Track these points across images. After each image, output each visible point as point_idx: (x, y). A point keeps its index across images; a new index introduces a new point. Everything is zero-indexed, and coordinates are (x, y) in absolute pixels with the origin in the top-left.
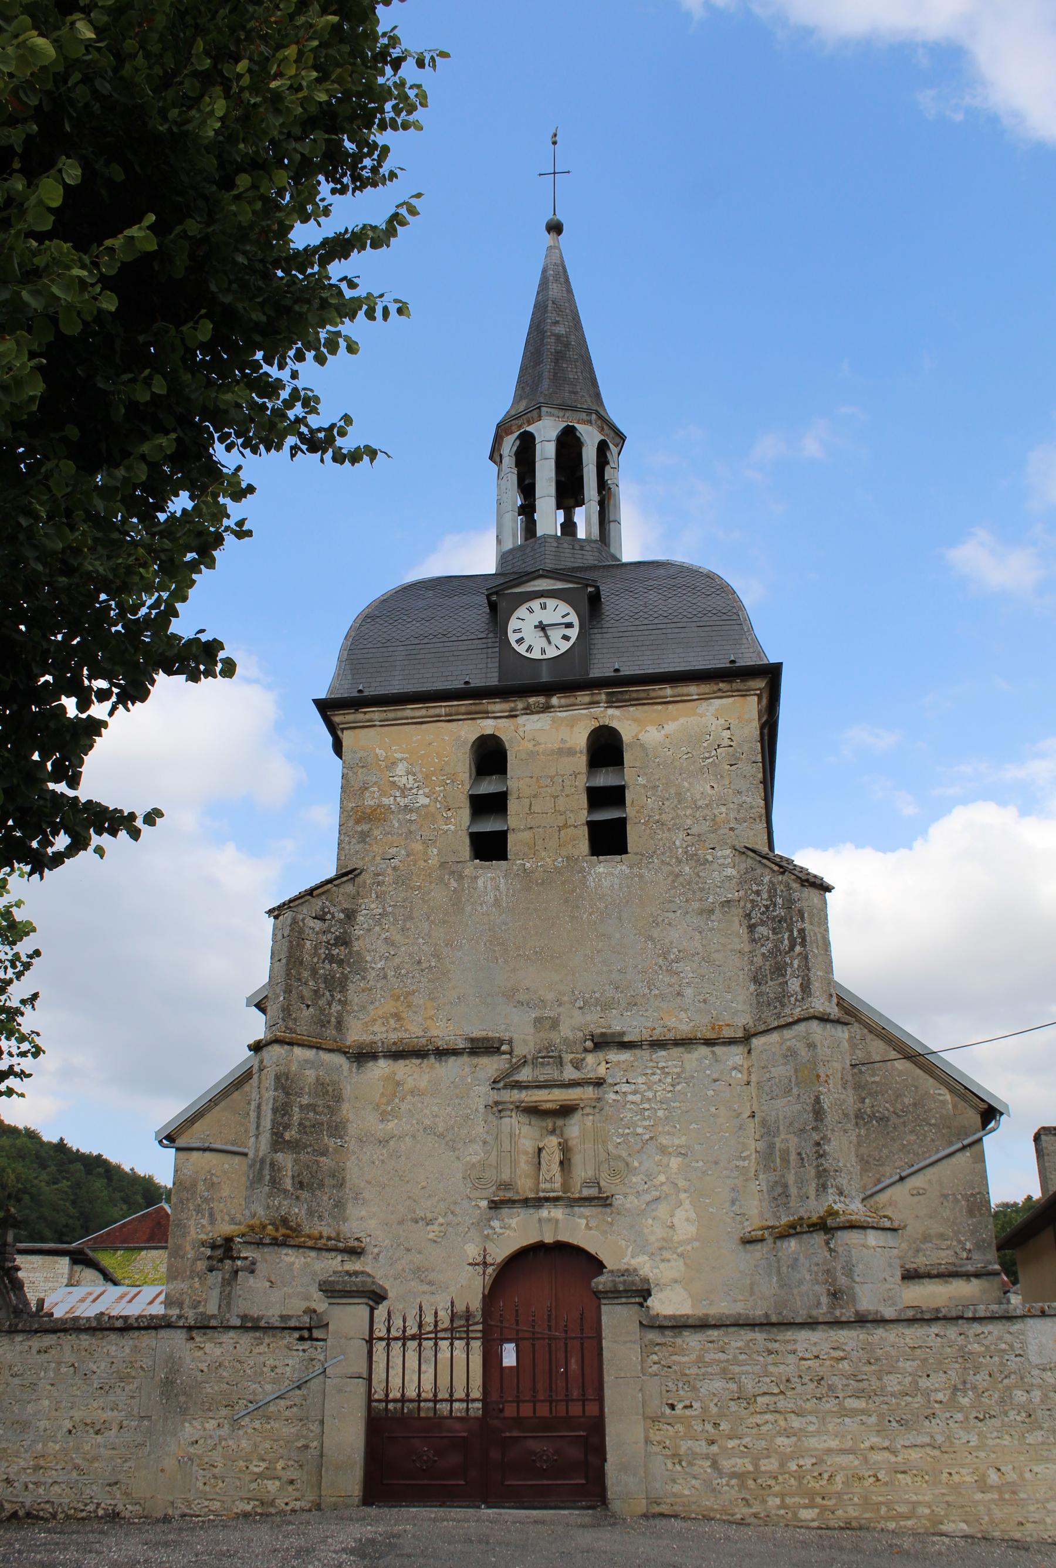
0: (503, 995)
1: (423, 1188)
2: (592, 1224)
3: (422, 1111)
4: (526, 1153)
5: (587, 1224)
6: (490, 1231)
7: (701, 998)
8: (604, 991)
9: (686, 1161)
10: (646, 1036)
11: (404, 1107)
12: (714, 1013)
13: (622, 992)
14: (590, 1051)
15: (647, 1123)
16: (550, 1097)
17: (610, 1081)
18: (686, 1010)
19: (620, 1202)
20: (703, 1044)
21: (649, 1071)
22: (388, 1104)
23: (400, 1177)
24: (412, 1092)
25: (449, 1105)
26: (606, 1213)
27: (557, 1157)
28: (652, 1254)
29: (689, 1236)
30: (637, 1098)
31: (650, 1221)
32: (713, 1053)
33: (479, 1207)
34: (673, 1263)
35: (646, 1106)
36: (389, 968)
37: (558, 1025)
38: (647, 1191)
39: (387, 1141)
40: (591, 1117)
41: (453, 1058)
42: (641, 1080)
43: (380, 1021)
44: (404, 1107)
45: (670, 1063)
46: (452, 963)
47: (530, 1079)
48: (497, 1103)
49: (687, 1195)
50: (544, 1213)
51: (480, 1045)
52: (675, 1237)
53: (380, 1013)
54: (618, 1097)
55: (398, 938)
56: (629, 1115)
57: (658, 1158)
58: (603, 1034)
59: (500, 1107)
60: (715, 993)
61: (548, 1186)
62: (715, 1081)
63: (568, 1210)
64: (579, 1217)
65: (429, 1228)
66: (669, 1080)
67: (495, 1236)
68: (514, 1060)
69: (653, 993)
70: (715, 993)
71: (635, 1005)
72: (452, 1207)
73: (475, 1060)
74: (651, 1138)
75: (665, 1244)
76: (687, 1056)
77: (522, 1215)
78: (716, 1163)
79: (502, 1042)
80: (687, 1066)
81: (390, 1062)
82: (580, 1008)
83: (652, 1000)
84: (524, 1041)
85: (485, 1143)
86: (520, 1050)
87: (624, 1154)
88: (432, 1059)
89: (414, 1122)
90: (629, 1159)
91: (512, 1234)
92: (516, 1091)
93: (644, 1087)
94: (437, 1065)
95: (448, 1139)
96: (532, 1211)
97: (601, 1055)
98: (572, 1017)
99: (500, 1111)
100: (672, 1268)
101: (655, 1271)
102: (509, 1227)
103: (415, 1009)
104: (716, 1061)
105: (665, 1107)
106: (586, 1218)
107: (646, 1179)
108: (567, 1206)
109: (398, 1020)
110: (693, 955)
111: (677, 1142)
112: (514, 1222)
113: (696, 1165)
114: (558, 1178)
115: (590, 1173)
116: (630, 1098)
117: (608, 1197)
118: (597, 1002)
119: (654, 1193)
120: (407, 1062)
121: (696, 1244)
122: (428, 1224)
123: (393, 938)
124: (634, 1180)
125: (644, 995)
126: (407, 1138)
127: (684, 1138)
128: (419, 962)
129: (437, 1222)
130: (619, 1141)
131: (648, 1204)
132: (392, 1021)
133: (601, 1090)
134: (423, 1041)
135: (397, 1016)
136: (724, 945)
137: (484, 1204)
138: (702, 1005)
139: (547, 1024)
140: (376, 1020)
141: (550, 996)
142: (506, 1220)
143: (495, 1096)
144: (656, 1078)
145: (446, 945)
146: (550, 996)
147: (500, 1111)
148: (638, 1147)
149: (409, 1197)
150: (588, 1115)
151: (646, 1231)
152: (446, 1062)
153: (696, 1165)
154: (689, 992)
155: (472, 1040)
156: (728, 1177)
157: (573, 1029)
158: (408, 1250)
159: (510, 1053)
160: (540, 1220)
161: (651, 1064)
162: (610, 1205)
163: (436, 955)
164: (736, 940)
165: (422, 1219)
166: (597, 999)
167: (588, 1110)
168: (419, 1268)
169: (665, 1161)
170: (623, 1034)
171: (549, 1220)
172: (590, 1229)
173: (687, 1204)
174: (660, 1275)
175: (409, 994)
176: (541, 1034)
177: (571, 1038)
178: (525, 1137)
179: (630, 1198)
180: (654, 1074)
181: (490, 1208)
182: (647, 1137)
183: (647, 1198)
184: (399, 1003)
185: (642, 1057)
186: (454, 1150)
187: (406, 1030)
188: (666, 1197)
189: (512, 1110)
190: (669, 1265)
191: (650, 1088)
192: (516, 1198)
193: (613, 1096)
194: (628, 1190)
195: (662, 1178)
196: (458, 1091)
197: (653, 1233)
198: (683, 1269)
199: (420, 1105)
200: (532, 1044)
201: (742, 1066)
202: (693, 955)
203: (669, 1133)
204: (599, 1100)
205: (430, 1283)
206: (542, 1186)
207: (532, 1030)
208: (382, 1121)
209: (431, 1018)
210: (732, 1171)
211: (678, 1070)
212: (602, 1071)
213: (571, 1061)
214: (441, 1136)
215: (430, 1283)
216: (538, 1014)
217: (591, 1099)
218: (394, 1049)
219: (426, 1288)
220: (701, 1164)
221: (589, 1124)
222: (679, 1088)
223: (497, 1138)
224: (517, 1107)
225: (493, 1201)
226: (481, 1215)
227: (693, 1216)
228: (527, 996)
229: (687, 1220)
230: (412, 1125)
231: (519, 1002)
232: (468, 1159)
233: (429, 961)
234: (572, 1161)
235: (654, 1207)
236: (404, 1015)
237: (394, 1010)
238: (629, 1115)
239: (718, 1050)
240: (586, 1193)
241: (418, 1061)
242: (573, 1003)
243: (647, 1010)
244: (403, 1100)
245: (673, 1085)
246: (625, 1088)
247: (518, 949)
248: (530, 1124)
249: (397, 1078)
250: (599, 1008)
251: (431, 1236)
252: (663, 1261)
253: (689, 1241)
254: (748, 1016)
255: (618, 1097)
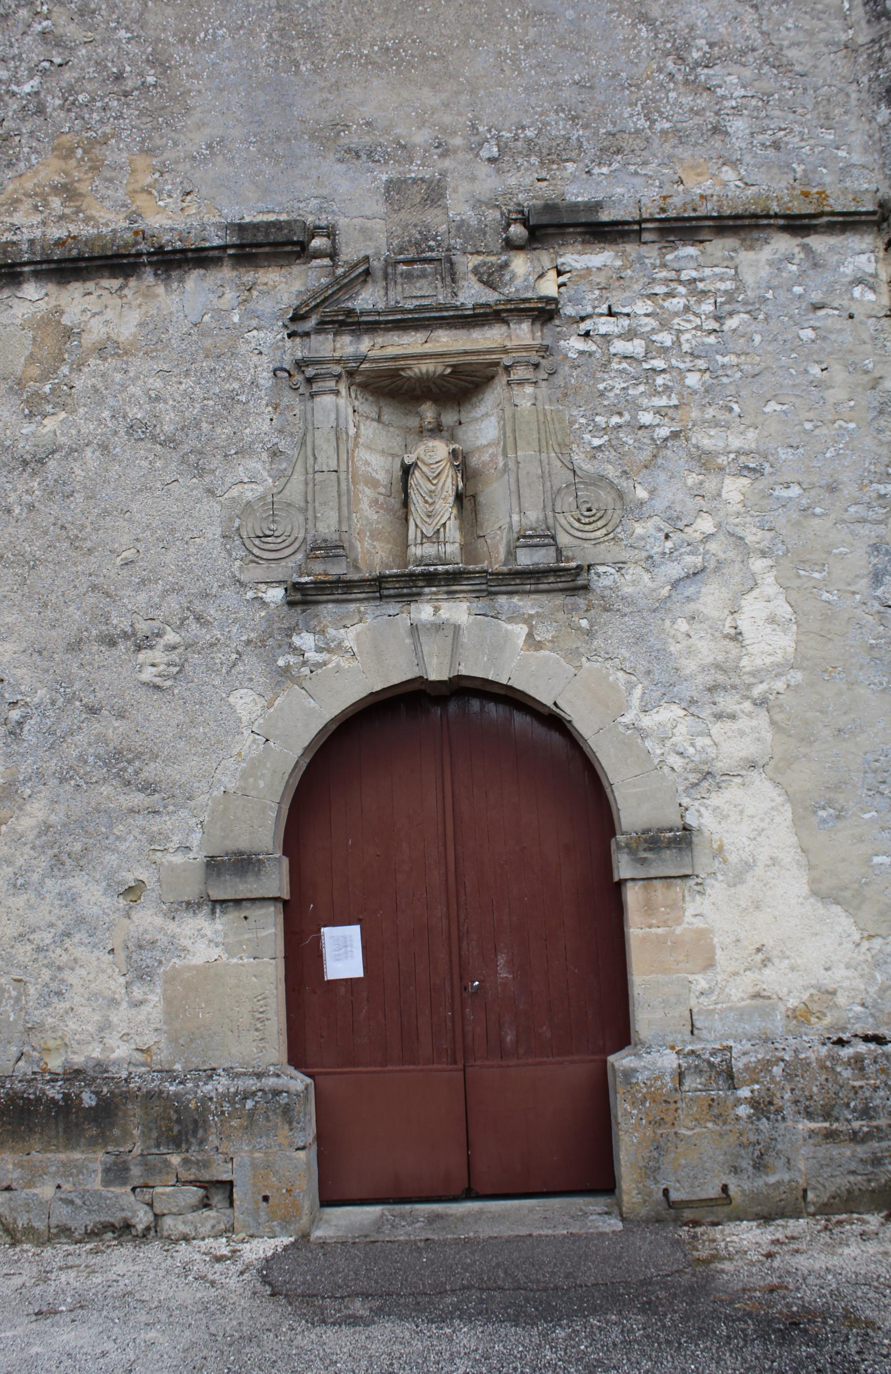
0: (313, 137)
1: (127, 563)
2: (544, 633)
3: (124, 387)
4: (374, 483)
5: (530, 635)
6: (292, 659)
7: (767, 138)
8: (546, 124)
9: (762, 484)
10: (650, 210)
11: (81, 382)
12: (800, 169)
13: (586, 127)
14: (520, 248)
15: (662, 401)
16: (428, 348)
17: (569, 310)
18: (734, 164)
19: (606, 582)
20: (784, 229)
21: (660, 289)
22: (44, 378)
23: (73, 542)
24: (101, 350)
25: (187, 373)
26: (575, 608)
27: (448, 484)
28: (693, 702)
29: (778, 658)
30: (637, 347)
31: (683, 626)
32: (806, 248)
33: (264, 604)
34: (743, 723)
35: (659, 364)
36: (49, 91)
37: (442, 196)
38: (670, 556)
39: (41, 461)
40: (529, 389)
41: (196, 274)
42: (642, 307)
43: (27, 204)
44: (81, 382)
45: (708, 272)
46: (196, 76)
47: (381, 306)
48: (300, 365)
49: (768, 562)
50: (424, 612)
51: (261, 238)
52: (744, 662)
53: (29, 186)
54: (590, 346)
55: (72, 31)
56: (619, 384)
57: (692, 479)
58: (550, 208)
59: (310, 371)
60: (797, 128)
61: (429, 550)
62: (817, 307)
63: (481, 605)
64: (510, 620)
65: (142, 656)
66: (707, 307)
67: (305, 670)
68: (340, 271)
69: (658, 126)
70: (797, 128)
71: (618, 152)
72: (198, 607)
73: (249, 276)
74: (675, 435)
75: (721, 678)
76: (745, 257)
77: (369, 619)
78: (832, 489)
79: (314, 232)
80: (749, 278)
81: (51, 288)
82: (492, 160)
83: (656, 142)
84: (363, 230)
85: (275, 453)
86: (349, 253)
87: (611, 472)
88: (149, 277)
89: (106, 414)
90: (624, 484)
91: (345, 664)
92: (347, 339)
93: (652, 323)
94: (161, 289)
95: (186, 448)
96: (393, 608)
97: (545, 258)
98: (473, 179)
99: (309, 381)
100: (742, 733)
101: (700, 741)
102: (339, 648)
103: (108, 174)
104: (815, 265)
105: (701, 364)
106: (527, 620)
107: (668, 528)
108: (478, 594)
109: (70, 198)
110: (743, 53)
111: (736, 443)
112: (350, 637)
113: (785, 493)
114: (453, 532)
115: (533, 516)
116: (619, 346)
117: (579, 568)
118: (531, 146)
119: (689, 559)
120: (90, 285)
121: (797, 677)
122: (139, 648)
123: (59, 31)
124: (639, 530)
125: (637, 131)
126: (88, 452)
127: (751, 434)
128: (119, 77)
129: (162, 641)
130: (596, 442)
131: (675, 584)
132: (56, 202)
133: (548, 330)
134: (128, 236)
135: (68, 192)
136: (811, 33)
137: (276, 595)
138: (771, 152)
139: (417, 194)
140: (18, 201)
141: (421, 137)
142: (331, 632)
143: (297, 350)
144: (676, 304)
145: (181, 41)
146: (421, 137)
147: (309, 381)
148: (645, 455)
149: (94, 587)
150: (521, 383)
151: (673, 648)
152: (181, 281)
153: (785, 493)
154: (738, 126)
155: (241, 228)
156: (863, 521)
157: (478, 204)
158: (93, 711)
159: (333, 255)
160: (414, 629)
161: (664, 274)
162: (586, 588)
163: (158, 62)
164: (837, 23)
165: (125, 635)
166: (529, 141)
167: (520, 373)
168: (118, 754)
169: (711, 485)
170: (597, 206)
171: (439, 627)
172: (539, 646)
173: (769, 585)
174: (712, 752)
175: (93, 142)
176: (403, 215)
177: (474, 222)
178: (369, 447)
179: (633, 572)
180: (670, 295)
181: (291, 604)
182: (664, 432)
183: (675, 570)
184: (73, 163)
185: (641, 259)
186: (200, 472)
187: (88, 219)
188: (717, 569)
189: (338, 377)
190: (735, 727)
191: (664, 325)
192: (356, 577)
193: (579, 344)
194: (625, 555)
195: (706, 525)
196: (208, 343)
197: (690, 652)
198: (768, 736)
199: (118, 377)
200: (382, 238)
201: (875, 276)
202: (743, 53)
203: (715, 423)
204: (546, 350)
205: (149, 788)
206: (416, 551)
207: (381, 208)
208: (31, 415)
209: (146, 190)
210: (869, 506)
211: (728, 285)
212: (549, 287)
213: (476, 271)
214: (171, 442)
215: (149, 788)
216: (394, 175)
217: (527, 348)
218: (57, 254)
219: (138, 799)
220: (795, 491)
221: (525, 404)
222: (732, 323)
223: (303, 443)
224: (351, 374)
225: (297, 587)
226: (269, 620)
227: (784, 610)
228: (367, 139)
229: (772, 620)
230: (100, 421)
231: (349, 150)
232: (234, 492)
233: (141, 75)
234: (482, 499)
235: (690, 590)
236: (84, 188)
237: (58, 179)
238: (619, 384)
239: (817, 242)
240: (525, 559)
241: (116, 283)
242: (475, 149)
243: (645, 163)
244: (78, 368)
245: (718, 319)
246: (605, 325)
247: (345, 43)
248: (379, 420)
249: (66, 320)
250: (534, 160)
251: (148, 675)
252: (719, 717)
253: (779, 670)
254: (877, 176)
255: (590, 346)
